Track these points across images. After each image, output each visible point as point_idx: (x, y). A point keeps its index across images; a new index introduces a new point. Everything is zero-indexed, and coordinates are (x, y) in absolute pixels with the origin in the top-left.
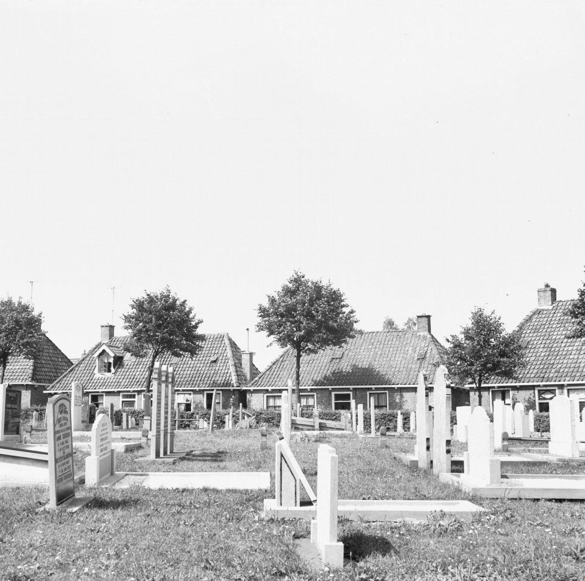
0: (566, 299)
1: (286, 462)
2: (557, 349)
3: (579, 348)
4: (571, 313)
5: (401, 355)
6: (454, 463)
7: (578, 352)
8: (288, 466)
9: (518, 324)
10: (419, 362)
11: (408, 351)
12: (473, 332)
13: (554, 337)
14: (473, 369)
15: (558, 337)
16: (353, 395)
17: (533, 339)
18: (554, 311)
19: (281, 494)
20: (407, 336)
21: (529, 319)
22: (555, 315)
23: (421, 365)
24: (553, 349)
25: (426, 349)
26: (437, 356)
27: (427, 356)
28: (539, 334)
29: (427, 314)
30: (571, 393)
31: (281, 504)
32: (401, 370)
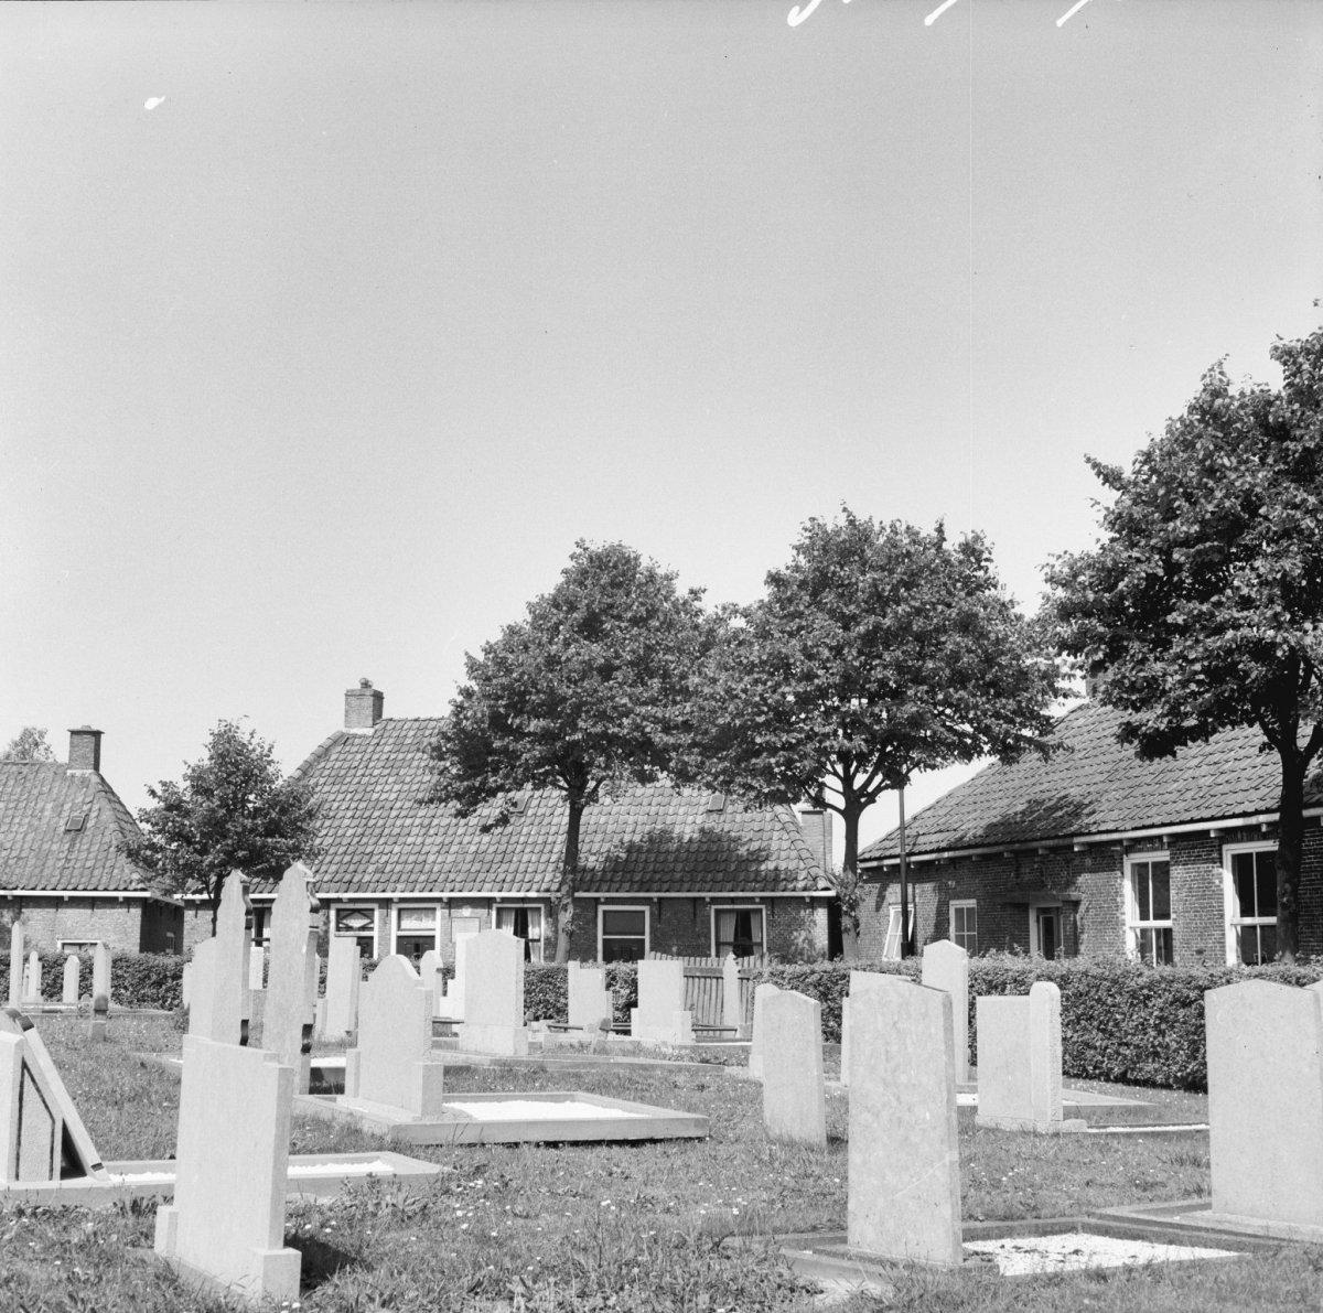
0: (403, 717)
1: (33, 1080)
2: (381, 822)
3: (427, 822)
4: (434, 749)
5: (27, 820)
6: (316, 1074)
7: (423, 831)
8: (38, 1090)
9: (300, 763)
10: (68, 837)
11: (42, 811)
12: (212, 777)
13: (375, 796)
14: (207, 862)
15: (384, 796)
16: (652, 914)
17: (332, 797)
18: (376, 741)
19: (18, 1154)
20: (41, 776)
21: (323, 754)
22: (379, 749)
23: (72, 845)
24: (372, 822)
25: (86, 808)
26: (113, 826)
27: (89, 825)
28: (344, 788)
29: (94, 728)
30: (404, 915)
31: (17, 1176)
32: (23, 855)
